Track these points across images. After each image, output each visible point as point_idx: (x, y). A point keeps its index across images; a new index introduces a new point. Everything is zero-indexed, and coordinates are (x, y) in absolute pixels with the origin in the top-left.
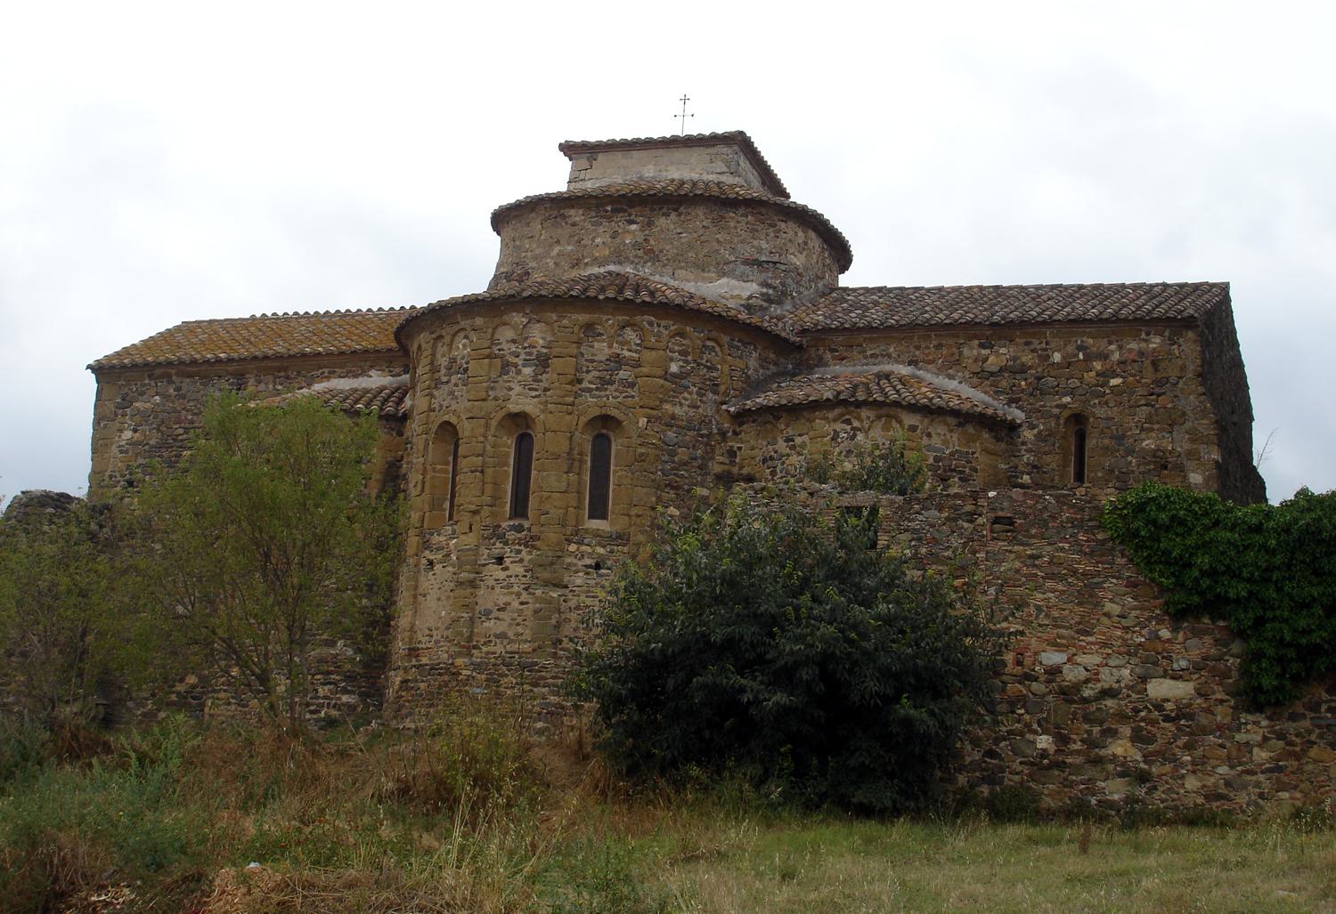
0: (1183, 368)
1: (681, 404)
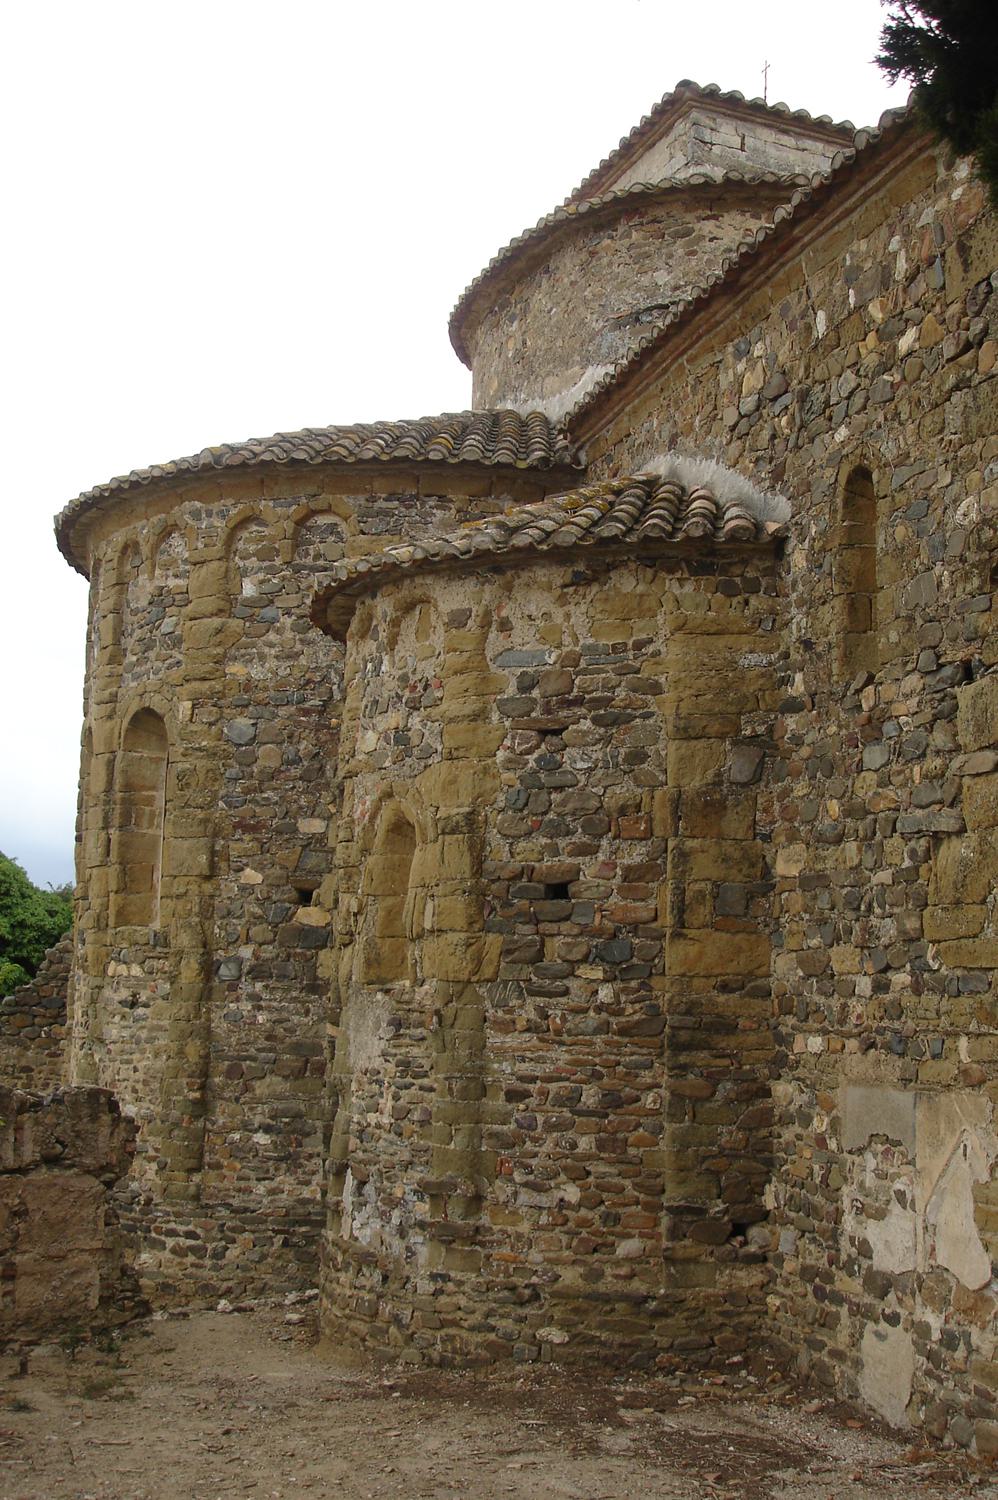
1: (262, 658)
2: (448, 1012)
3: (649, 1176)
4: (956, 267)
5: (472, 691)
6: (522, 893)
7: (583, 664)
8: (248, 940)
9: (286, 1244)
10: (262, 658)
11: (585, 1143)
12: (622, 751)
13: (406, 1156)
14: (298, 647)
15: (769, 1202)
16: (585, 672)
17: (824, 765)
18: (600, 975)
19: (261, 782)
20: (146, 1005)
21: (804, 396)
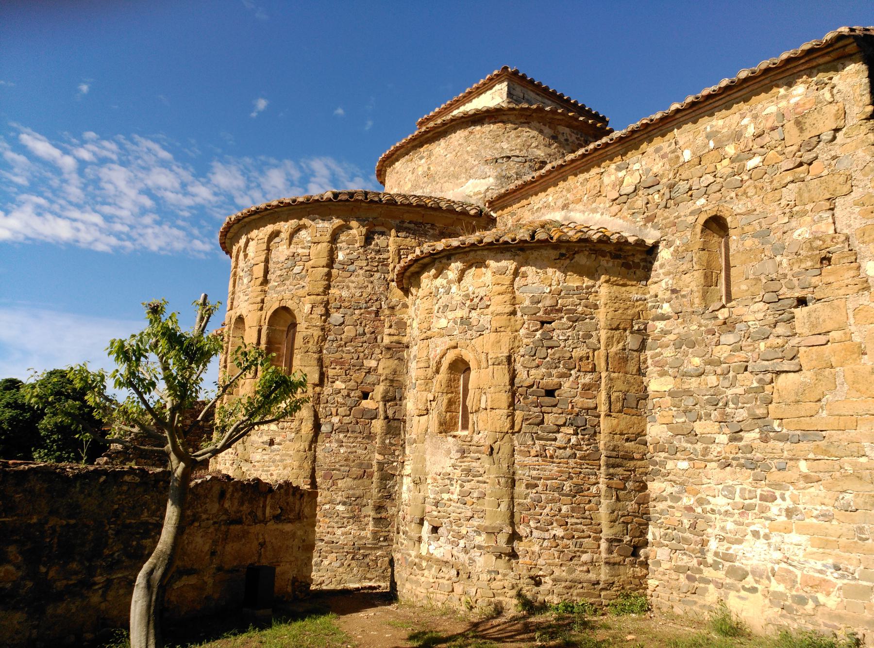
1: (348, 287)
2: (496, 447)
3: (595, 525)
5: (508, 303)
7: (562, 294)
8: (337, 415)
9: (353, 559)
12: (581, 333)
14: (366, 284)
16: (563, 298)
18: (572, 432)
19: (346, 344)
20: (279, 444)
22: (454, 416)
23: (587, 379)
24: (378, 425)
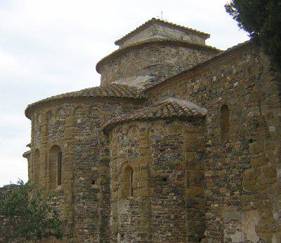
0: (262, 69)
1: (83, 135)
4: (247, 73)
6: (158, 180)
10: (83, 135)
11: (172, 225)
13: (135, 229)
15: (205, 234)
17: (216, 156)
21: (210, 91)
22: (129, 191)
23: (179, 173)
24: (99, 195)
